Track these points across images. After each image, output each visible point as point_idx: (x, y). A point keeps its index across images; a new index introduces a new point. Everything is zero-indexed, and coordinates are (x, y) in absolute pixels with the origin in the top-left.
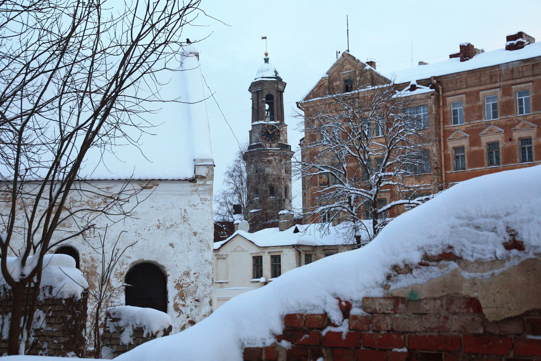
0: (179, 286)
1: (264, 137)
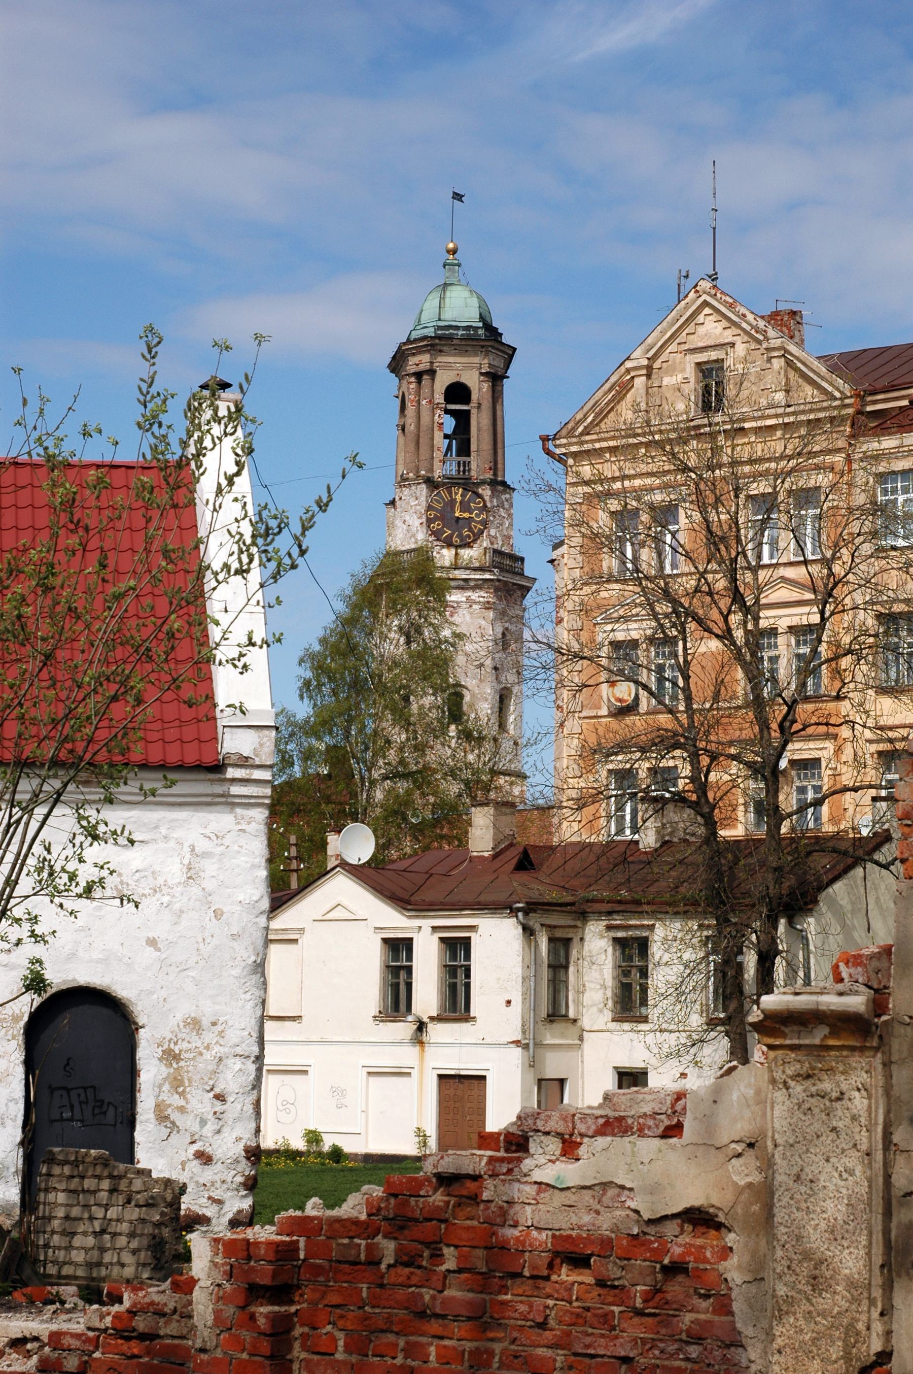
0: (171, 1056)
1: (435, 526)
